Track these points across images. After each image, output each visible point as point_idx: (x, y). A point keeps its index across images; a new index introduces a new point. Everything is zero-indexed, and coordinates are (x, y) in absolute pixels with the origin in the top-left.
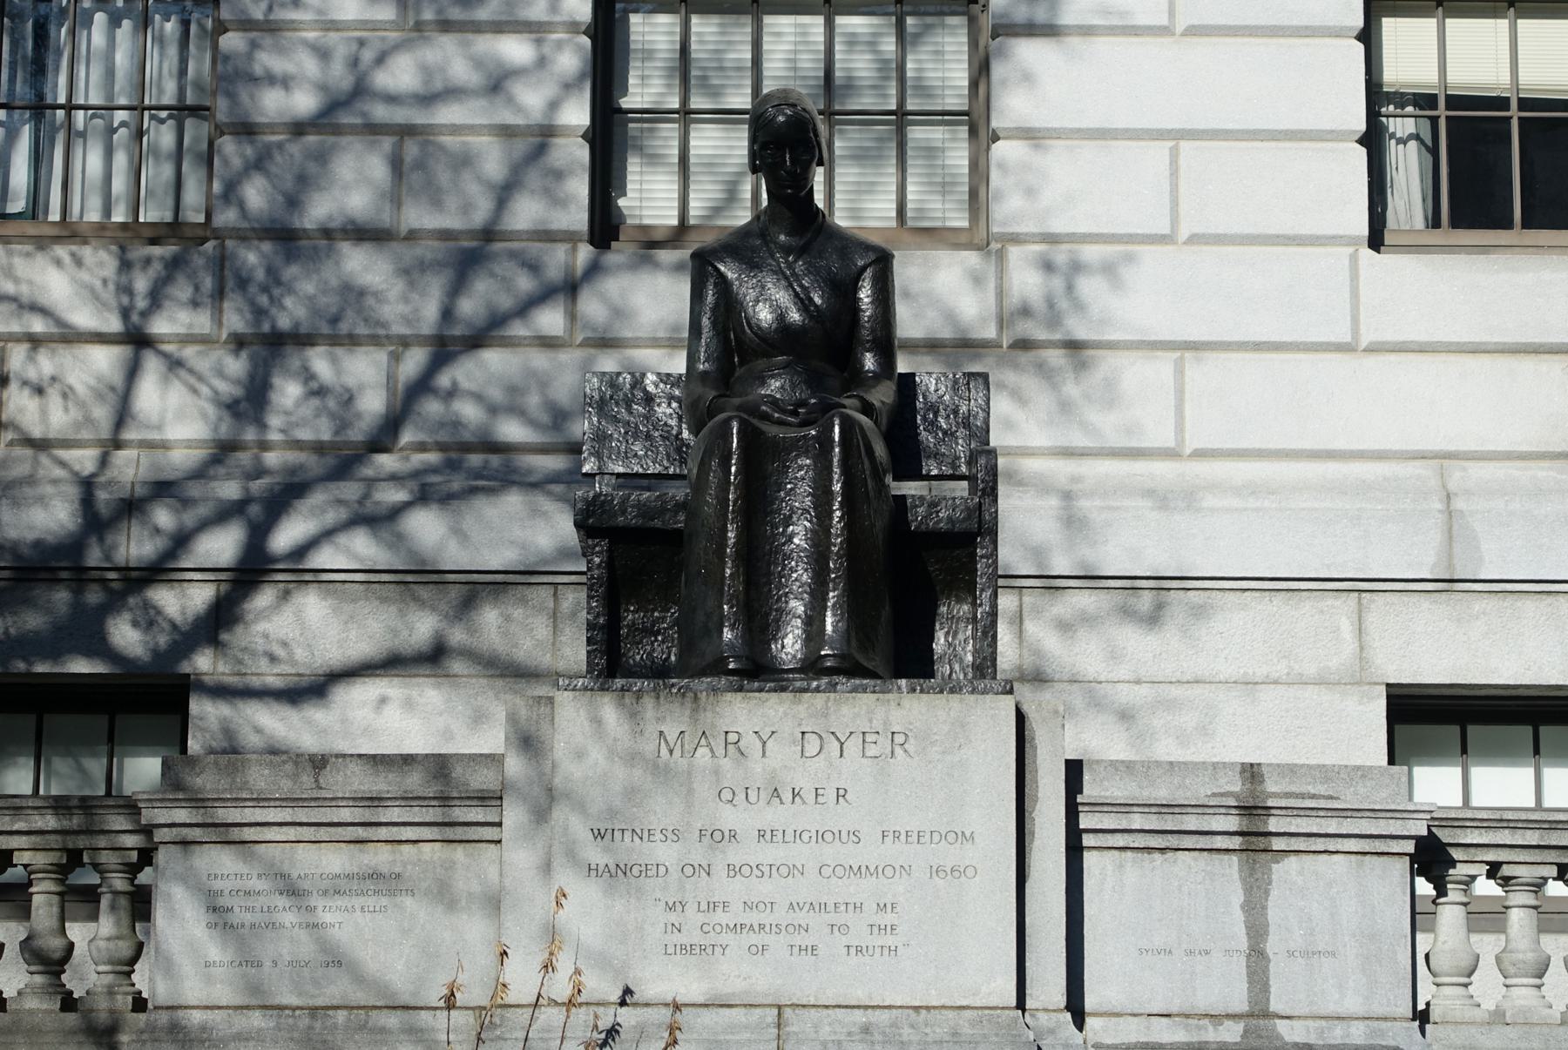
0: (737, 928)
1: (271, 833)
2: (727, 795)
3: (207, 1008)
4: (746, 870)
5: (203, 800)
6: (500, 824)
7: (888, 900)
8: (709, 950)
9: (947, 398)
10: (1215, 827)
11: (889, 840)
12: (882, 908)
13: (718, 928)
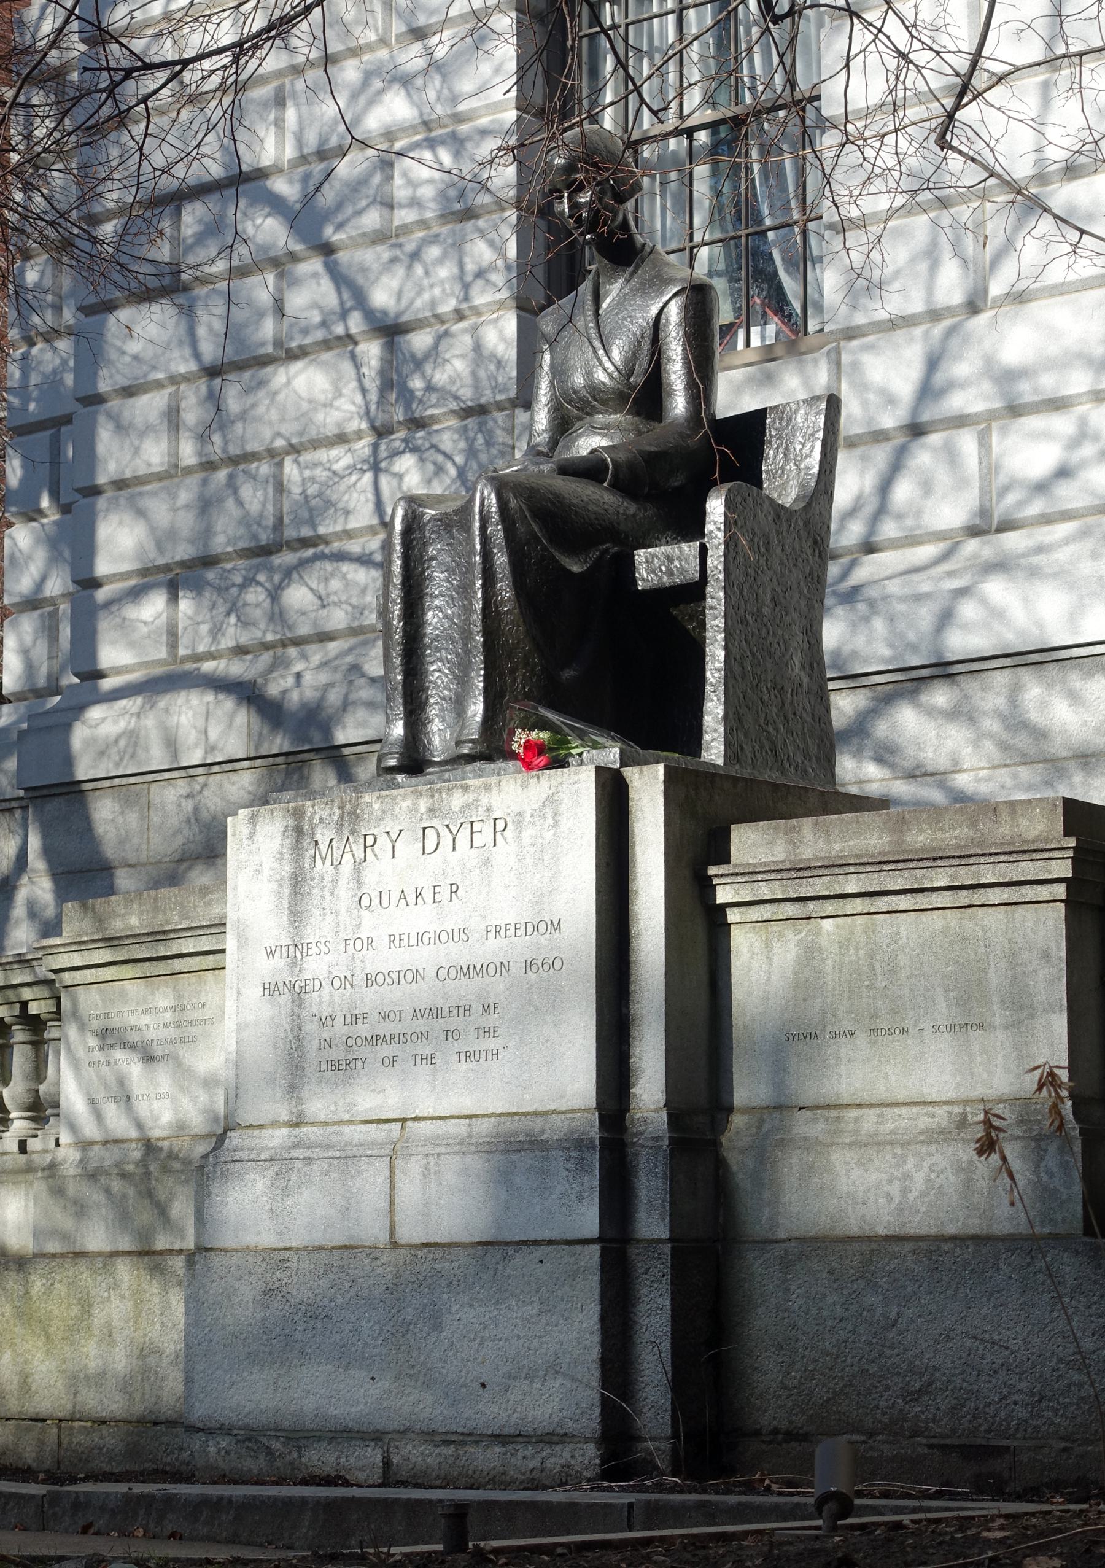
0: (373, 1040)
1: (89, 975)
2: (365, 901)
3: (379, 1121)
4: (380, 978)
5: (164, 932)
6: (223, 951)
7: (491, 1001)
8: (352, 1065)
9: (108, 229)
10: (850, 889)
11: (491, 935)
12: (486, 1009)
13: (359, 1041)
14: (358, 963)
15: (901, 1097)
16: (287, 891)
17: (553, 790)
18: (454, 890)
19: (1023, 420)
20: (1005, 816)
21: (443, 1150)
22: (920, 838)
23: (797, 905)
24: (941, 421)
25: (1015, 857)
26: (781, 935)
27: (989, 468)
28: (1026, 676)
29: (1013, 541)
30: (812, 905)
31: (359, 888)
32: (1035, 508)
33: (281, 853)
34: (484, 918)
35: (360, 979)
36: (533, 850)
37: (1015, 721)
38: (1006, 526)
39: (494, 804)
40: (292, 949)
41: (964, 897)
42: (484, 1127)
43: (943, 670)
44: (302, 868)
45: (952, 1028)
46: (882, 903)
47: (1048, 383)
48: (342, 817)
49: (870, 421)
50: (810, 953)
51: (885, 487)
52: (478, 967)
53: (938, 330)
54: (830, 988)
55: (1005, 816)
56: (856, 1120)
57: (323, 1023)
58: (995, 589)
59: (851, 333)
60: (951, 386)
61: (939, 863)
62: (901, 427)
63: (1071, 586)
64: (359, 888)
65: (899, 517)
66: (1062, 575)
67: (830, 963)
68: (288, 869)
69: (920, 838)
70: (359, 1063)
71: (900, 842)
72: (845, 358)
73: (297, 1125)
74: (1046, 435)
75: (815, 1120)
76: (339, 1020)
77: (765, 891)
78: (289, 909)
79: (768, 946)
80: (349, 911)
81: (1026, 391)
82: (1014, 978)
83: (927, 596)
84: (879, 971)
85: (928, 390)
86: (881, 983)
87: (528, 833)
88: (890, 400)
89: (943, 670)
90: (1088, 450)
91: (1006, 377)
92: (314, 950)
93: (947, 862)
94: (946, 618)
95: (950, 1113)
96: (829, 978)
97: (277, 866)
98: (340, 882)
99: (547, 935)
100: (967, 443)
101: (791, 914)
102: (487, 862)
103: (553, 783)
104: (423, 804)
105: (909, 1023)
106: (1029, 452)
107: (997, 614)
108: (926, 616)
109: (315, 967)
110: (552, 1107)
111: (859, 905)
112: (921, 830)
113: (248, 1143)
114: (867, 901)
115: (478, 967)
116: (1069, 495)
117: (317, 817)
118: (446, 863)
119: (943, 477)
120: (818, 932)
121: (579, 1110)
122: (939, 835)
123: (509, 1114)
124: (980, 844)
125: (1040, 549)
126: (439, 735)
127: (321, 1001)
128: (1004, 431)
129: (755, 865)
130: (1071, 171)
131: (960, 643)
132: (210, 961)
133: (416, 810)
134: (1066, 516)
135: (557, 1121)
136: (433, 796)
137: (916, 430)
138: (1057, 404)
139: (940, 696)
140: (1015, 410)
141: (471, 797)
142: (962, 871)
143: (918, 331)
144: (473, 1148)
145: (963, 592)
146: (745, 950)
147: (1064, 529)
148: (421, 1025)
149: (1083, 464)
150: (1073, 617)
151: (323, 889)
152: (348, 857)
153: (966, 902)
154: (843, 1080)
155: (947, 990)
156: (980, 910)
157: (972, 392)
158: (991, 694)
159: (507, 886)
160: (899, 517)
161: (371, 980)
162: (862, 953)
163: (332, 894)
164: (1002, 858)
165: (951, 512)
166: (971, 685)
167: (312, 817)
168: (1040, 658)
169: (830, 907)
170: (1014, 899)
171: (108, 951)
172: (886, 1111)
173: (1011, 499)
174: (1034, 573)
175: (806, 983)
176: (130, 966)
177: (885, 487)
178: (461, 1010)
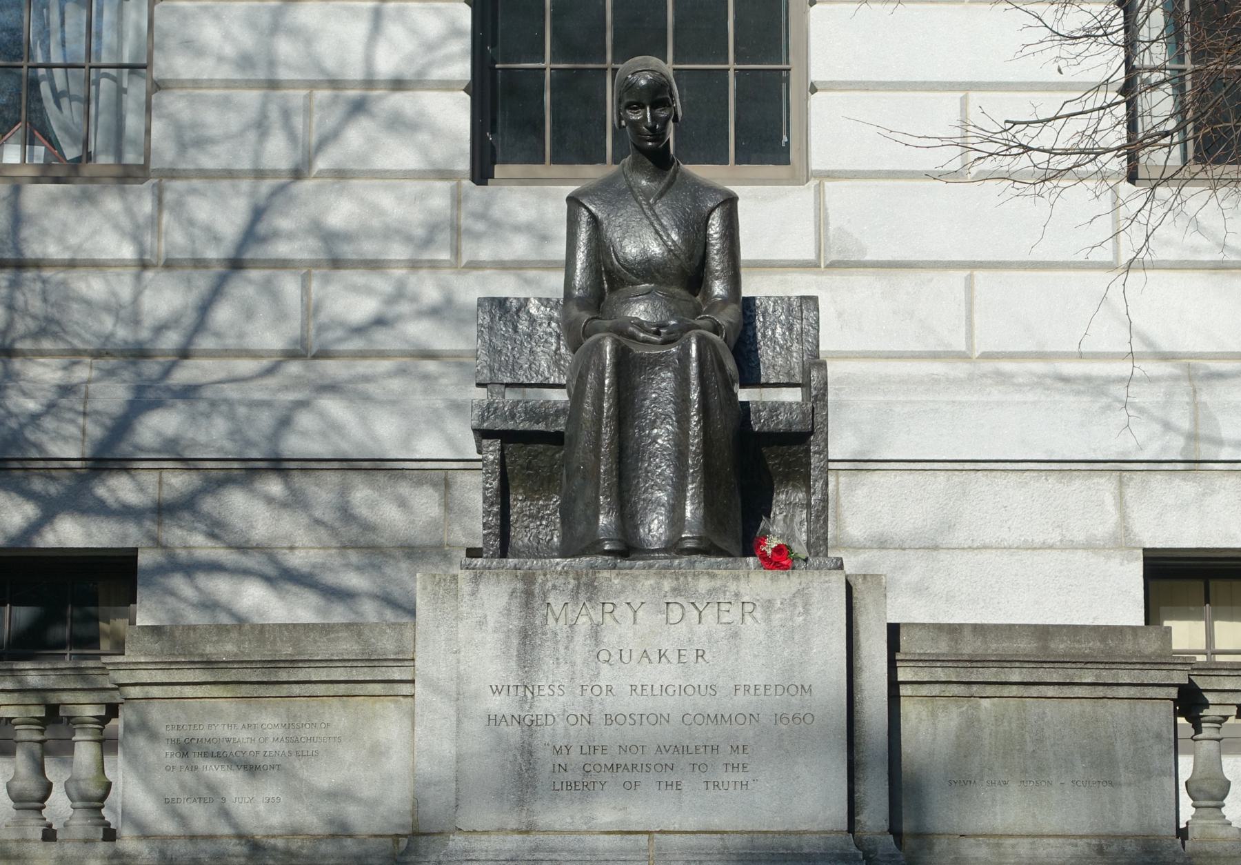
0: (615, 767)
2: (604, 656)
13: (598, 768)
14: (596, 705)
15: (1046, 831)
16: (515, 642)
17: (804, 585)
18: (700, 655)
19: (343, 272)
20: (1129, 637)
21: (703, 858)
22: (1061, 646)
23: (963, 687)
24: (265, 261)
25: (1147, 667)
26: (945, 708)
27: (311, 310)
28: (356, 479)
29: (333, 369)
30: (975, 688)
31: (597, 646)
32: (356, 344)
33: (509, 610)
34: (733, 679)
35: (597, 718)
36: (783, 630)
37: (346, 513)
38: (324, 354)
39: (742, 591)
40: (521, 689)
41: (1100, 691)
42: (736, 841)
43: (277, 465)
44: (533, 624)
45: (1087, 783)
46: (1034, 691)
47: (369, 249)
48: (578, 587)
49: (194, 252)
50: (971, 723)
51: (205, 307)
52: (726, 717)
53: (266, 186)
54: (987, 749)
55: (1129, 637)
56: (1013, 846)
57: (556, 751)
58: (334, 407)
59: (173, 174)
60: (275, 235)
61: (1089, 666)
62: (225, 260)
63: (405, 414)
64: (597, 646)
65: (217, 335)
66: (394, 403)
67: (987, 731)
68: (516, 623)
69: (1061, 646)
70: (598, 786)
71: (1045, 648)
72: (169, 197)
73: (527, 832)
74: (368, 291)
75: (978, 845)
76: (575, 752)
77: (941, 674)
78: (518, 656)
79: (933, 714)
80: (586, 662)
81: (348, 251)
82: (1136, 750)
83: (267, 404)
84: (1028, 739)
85: (251, 235)
86: (1030, 748)
87: (777, 618)
88: (216, 239)
89: (277, 465)
90: (404, 308)
91: (329, 237)
92: (547, 691)
93: (1095, 666)
94: (285, 423)
95: (1089, 844)
96: (987, 742)
97: (503, 620)
98: (576, 639)
99: (798, 697)
100: (290, 286)
101: (956, 693)
102: (735, 635)
103: (804, 580)
104: (667, 585)
105: (1053, 778)
106: (352, 302)
107: (335, 427)
108: (265, 420)
109: (547, 704)
110: (803, 827)
111: (1014, 690)
112: (1063, 641)
113: (477, 846)
114: (1021, 688)
115: (726, 717)
116: (383, 339)
117: (550, 584)
118: (691, 631)
119: (264, 307)
120: (978, 707)
121: (831, 832)
122: (1077, 646)
123: (760, 832)
124: (1160, 656)
125: (367, 379)
126: (655, 528)
127: (545, 735)
128: (326, 281)
129: (938, 655)
130: (398, 84)
131: (295, 445)
132: (405, 689)
133: (660, 589)
134: (382, 355)
135: (814, 839)
136: (677, 579)
137: (236, 264)
138: (374, 265)
139: (274, 487)
140: (336, 263)
141: (718, 583)
142: (1104, 673)
143: (245, 185)
144: (734, 858)
145: (302, 404)
146: (913, 717)
147: (385, 365)
148: (666, 758)
149: (399, 318)
150: (408, 438)
151: (557, 642)
152: (583, 619)
153: (1101, 695)
154: (999, 817)
155: (1083, 756)
156: (1109, 701)
157: (296, 245)
158: (322, 492)
159: (755, 656)
160: (217, 335)
161: (610, 719)
162: (1014, 726)
163: (567, 648)
164: (1138, 666)
165: (270, 338)
166: (299, 481)
167: (543, 584)
168: (376, 467)
169: (990, 690)
170: (1138, 695)
171: (208, 672)
172: (1037, 840)
173: (330, 335)
174: (367, 398)
175: (966, 746)
176: (222, 686)
177: (205, 307)
178: (709, 749)
